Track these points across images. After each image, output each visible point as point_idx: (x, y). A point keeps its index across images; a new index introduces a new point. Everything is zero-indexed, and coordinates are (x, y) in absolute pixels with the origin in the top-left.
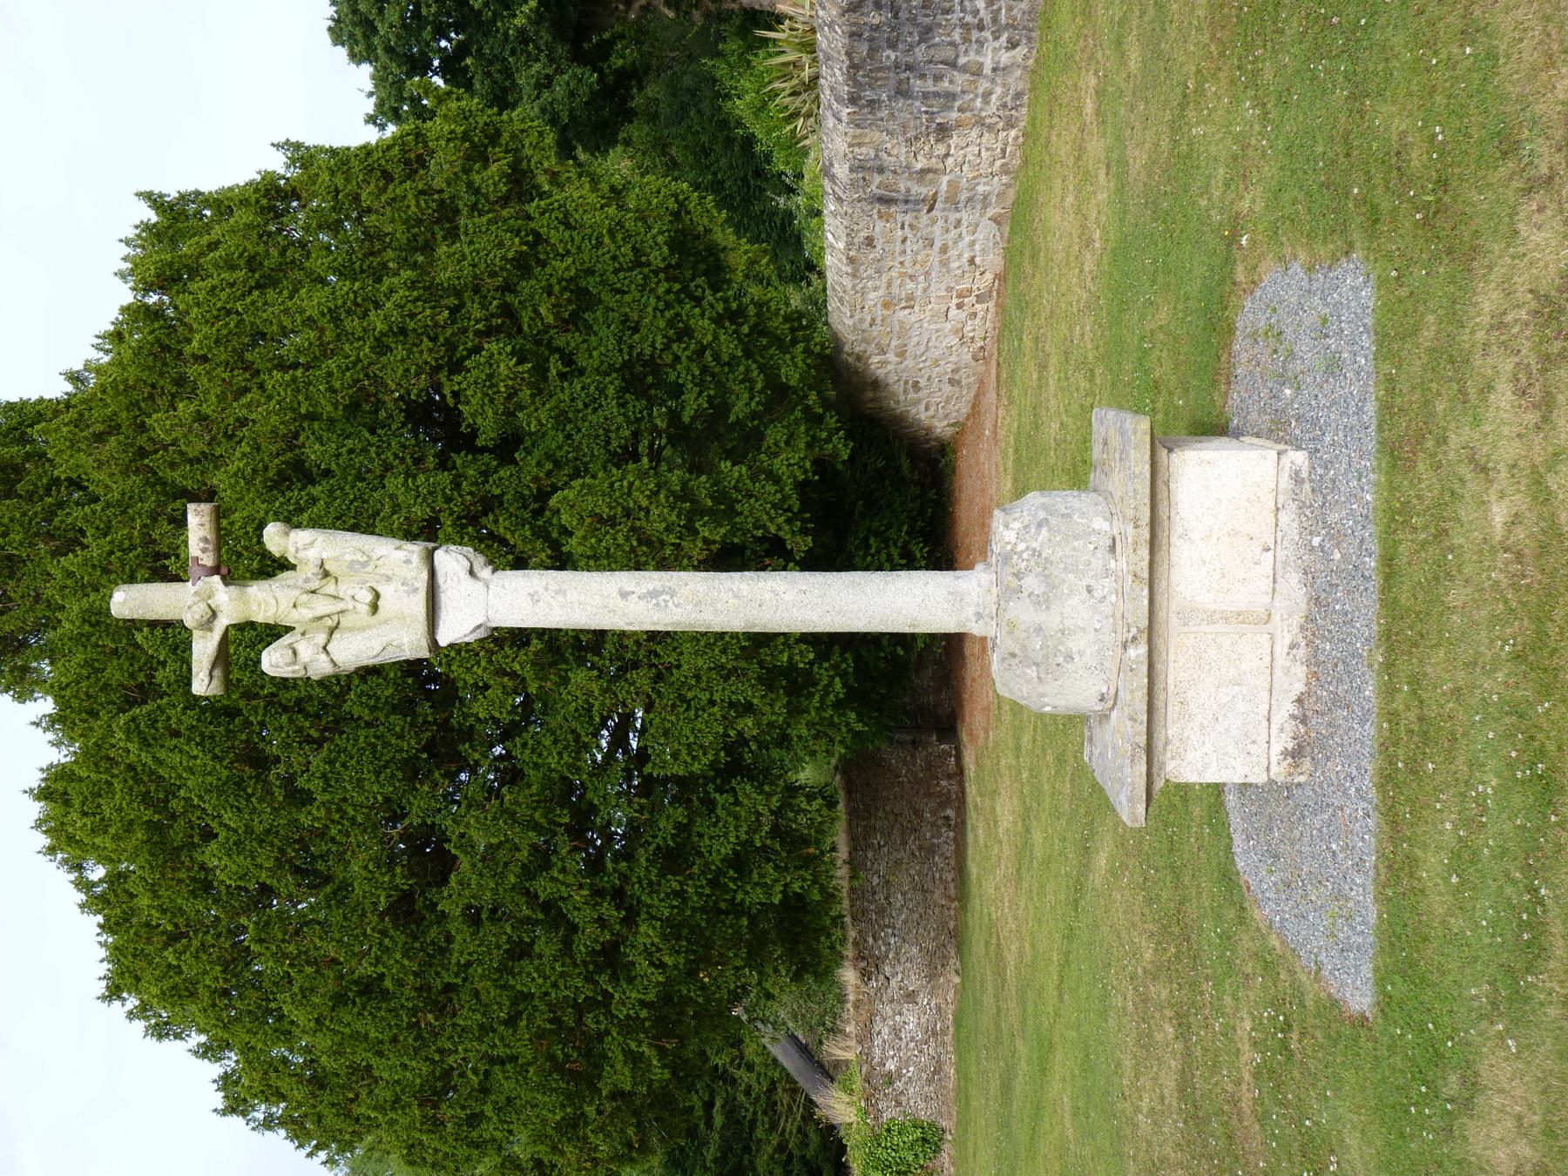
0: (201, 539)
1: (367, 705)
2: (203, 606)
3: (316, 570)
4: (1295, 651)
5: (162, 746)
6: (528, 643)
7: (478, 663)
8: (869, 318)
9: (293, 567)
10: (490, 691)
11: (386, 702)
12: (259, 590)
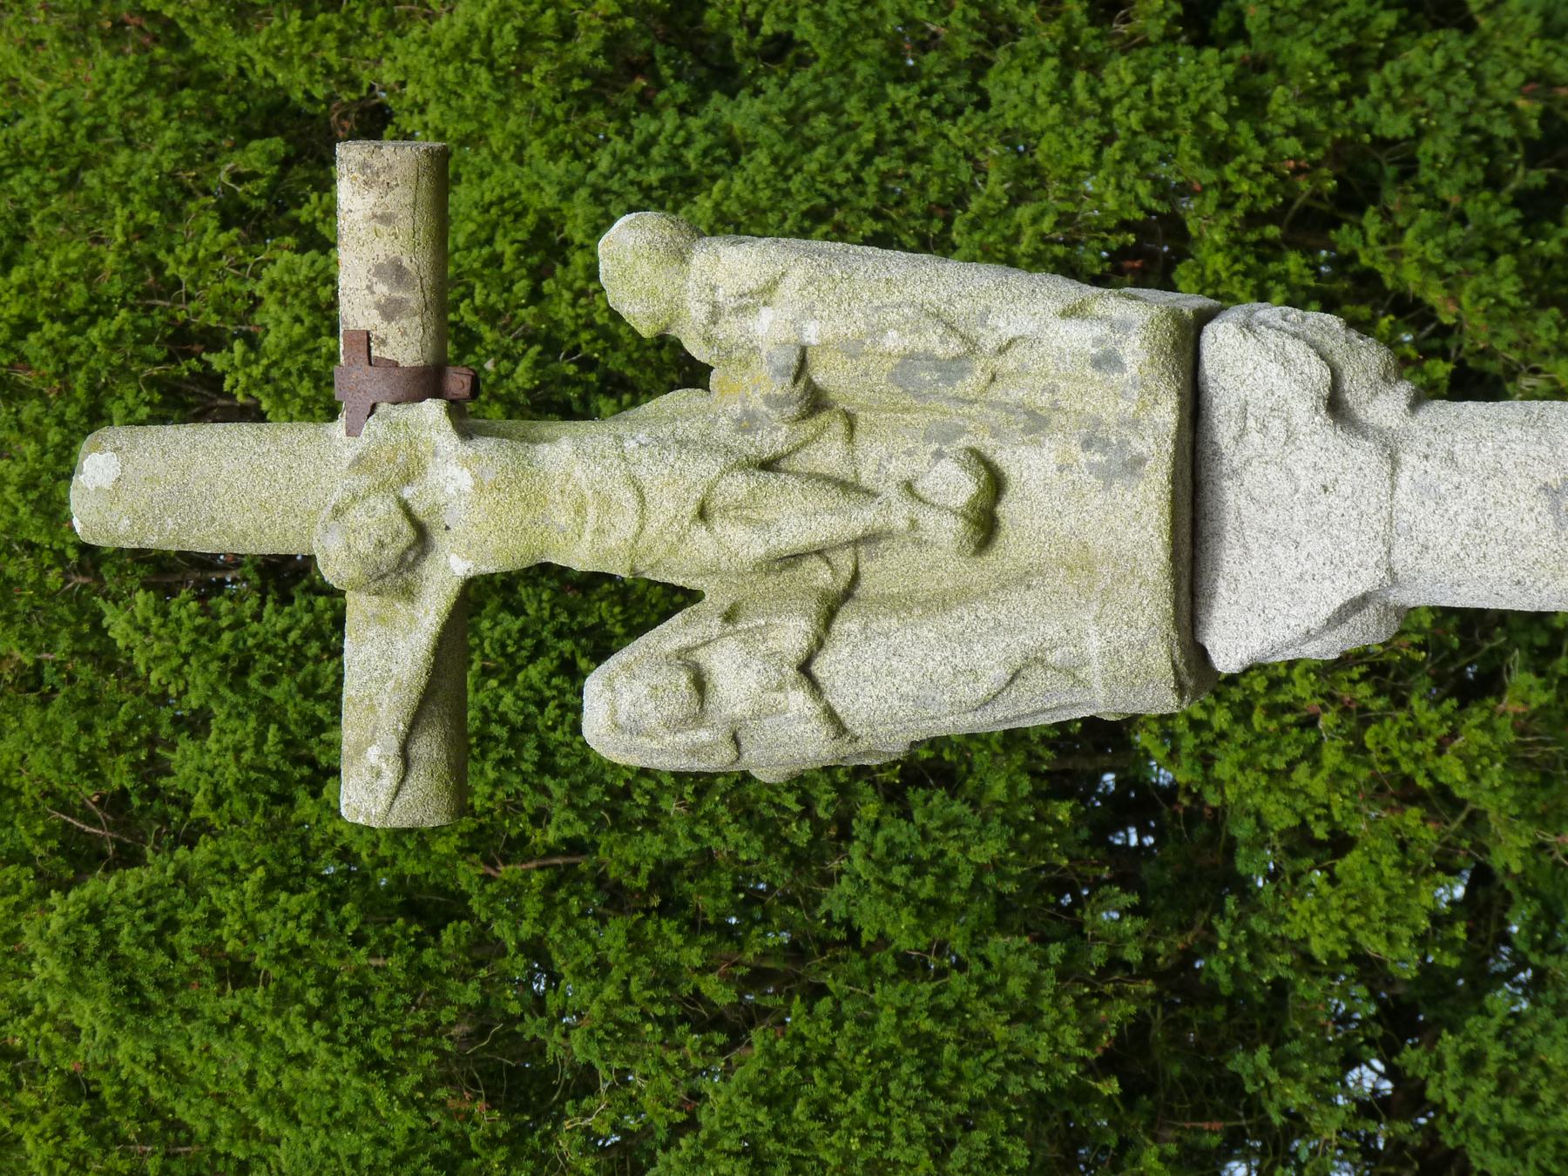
0: (379, 271)
1: (910, 897)
2: (384, 506)
3: (780, 386)
5: (189, 1015)
6: (1490, 684)
7: (1312, 755)
9: (695, 375)
10: (1353, 859)
11: (977, 886)
12: (580, 452)
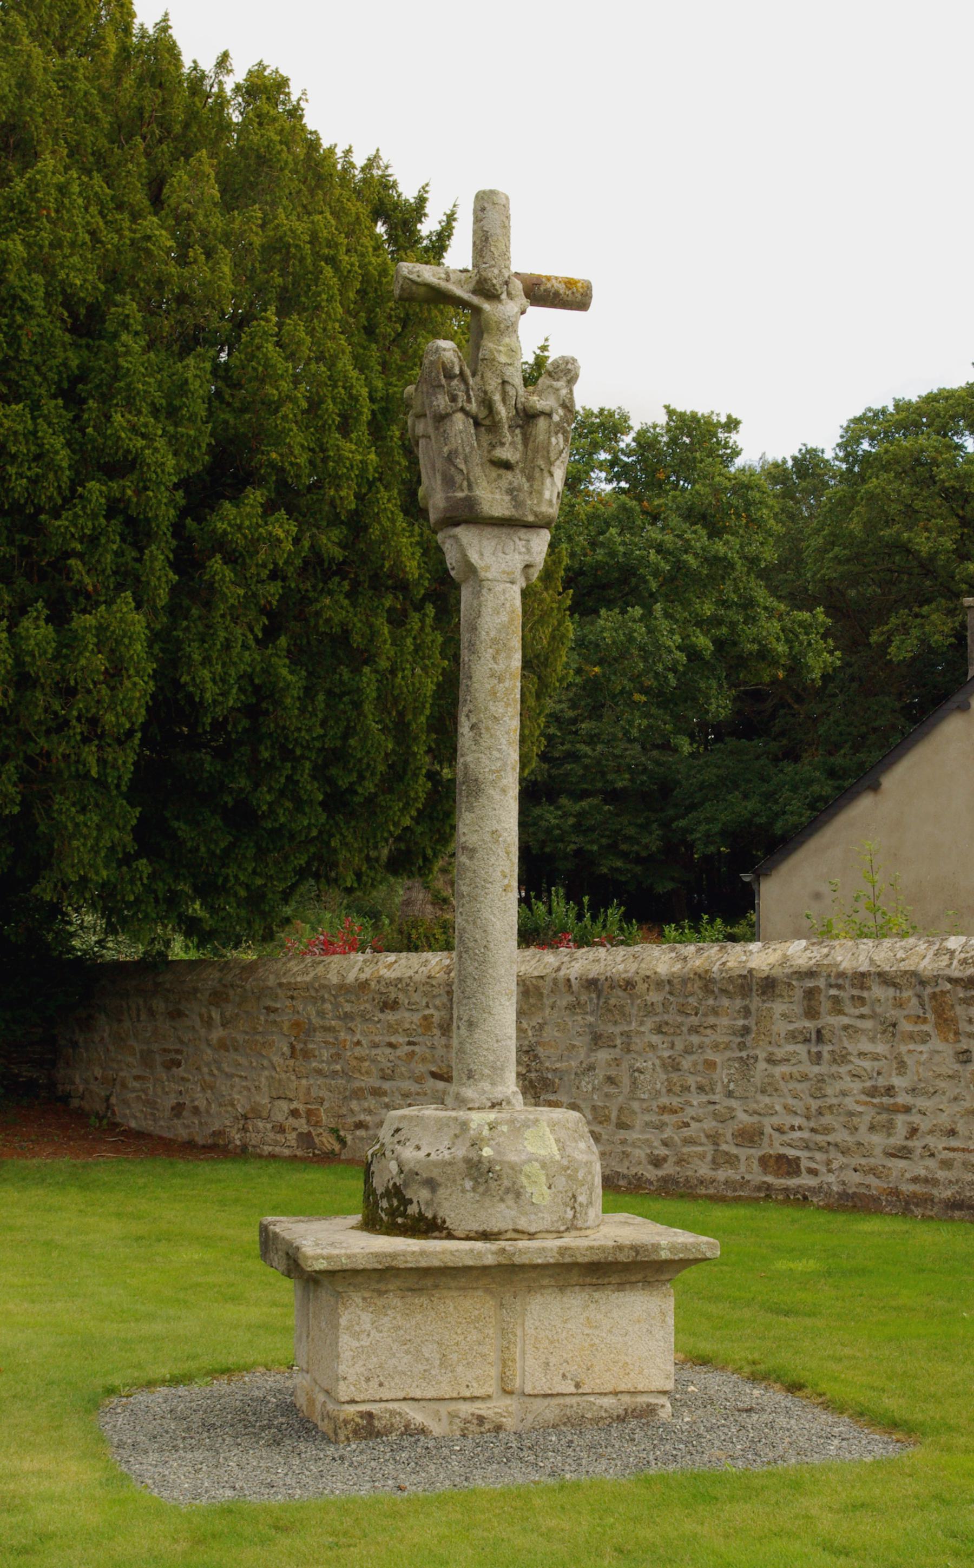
4: (475, 1421)
8: (278, 1006)
